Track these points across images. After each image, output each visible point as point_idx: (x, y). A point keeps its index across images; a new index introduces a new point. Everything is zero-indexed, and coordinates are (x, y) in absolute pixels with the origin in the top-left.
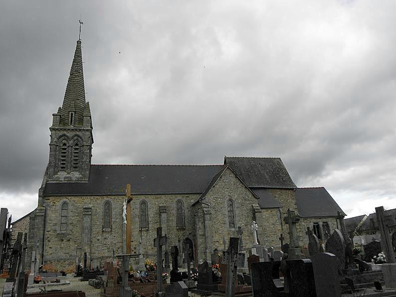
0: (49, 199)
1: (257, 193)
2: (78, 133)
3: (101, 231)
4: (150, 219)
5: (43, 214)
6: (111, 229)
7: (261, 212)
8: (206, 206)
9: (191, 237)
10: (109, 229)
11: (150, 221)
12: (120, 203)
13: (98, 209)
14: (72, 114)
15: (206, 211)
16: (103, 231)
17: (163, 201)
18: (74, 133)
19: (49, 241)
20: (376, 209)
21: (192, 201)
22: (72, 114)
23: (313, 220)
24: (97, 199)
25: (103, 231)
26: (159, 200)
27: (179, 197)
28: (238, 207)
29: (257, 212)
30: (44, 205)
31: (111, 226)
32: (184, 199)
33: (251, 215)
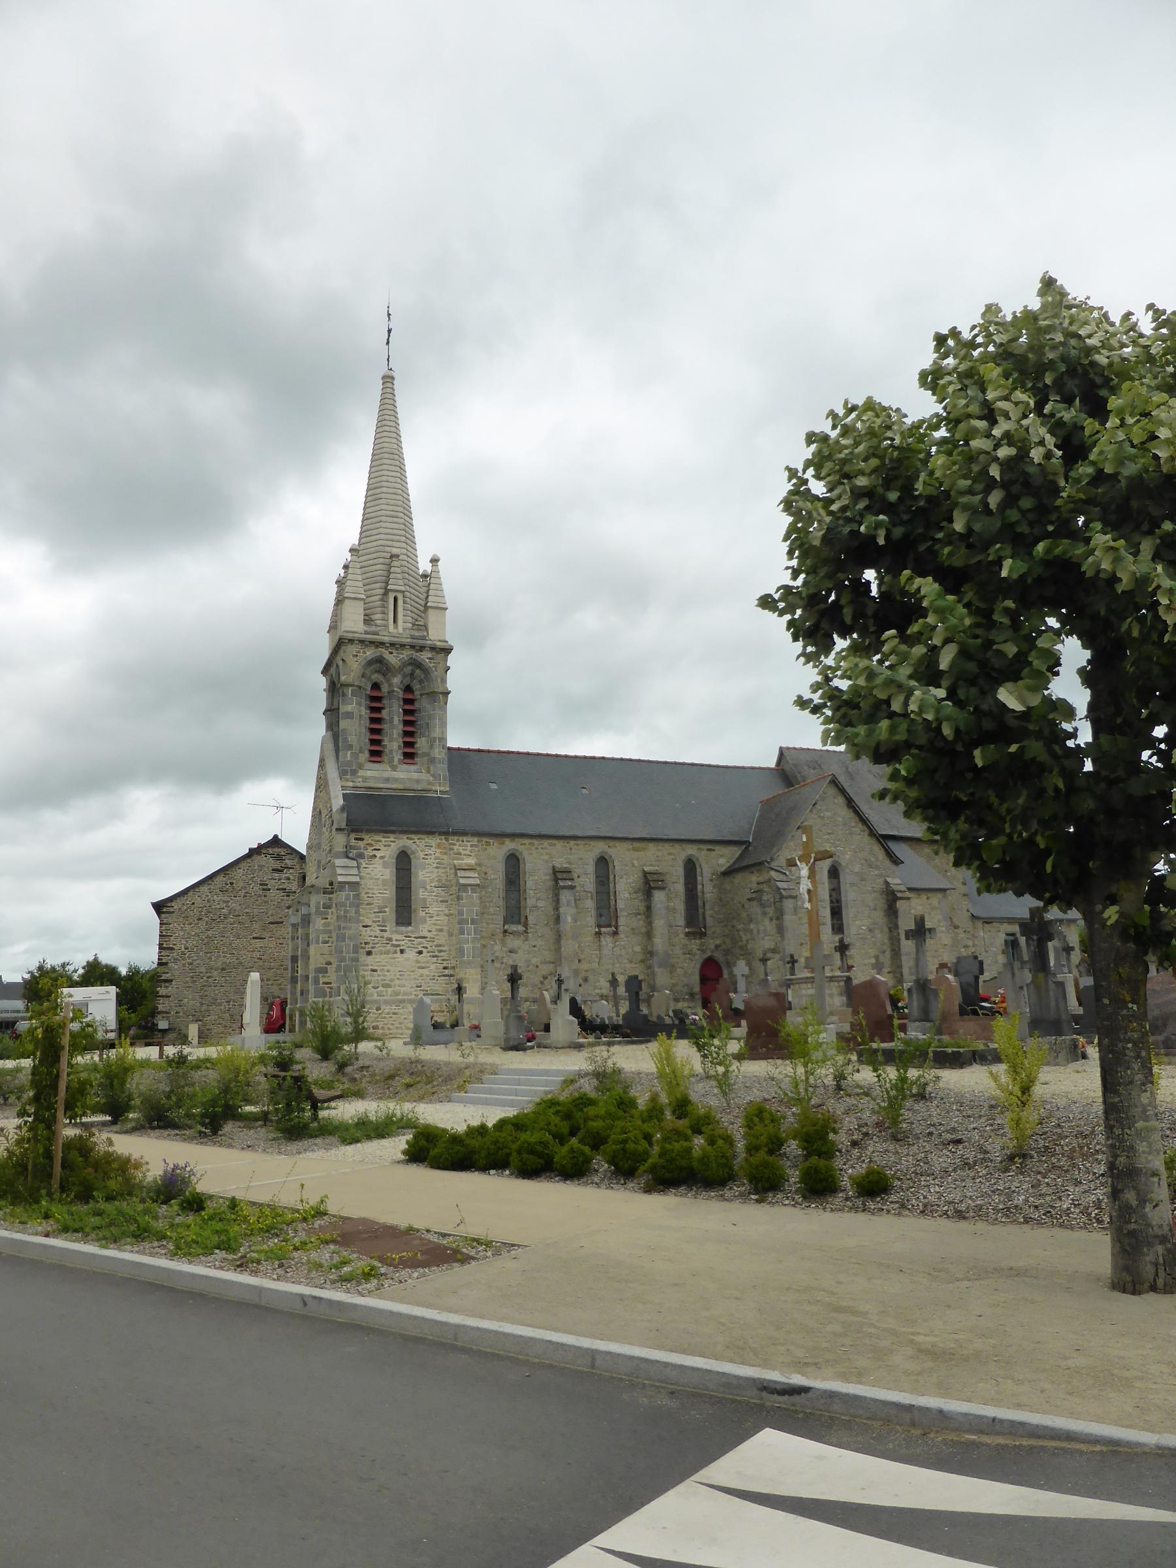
0: (362, 839)
1: (898, 849)
2: (416, 655)
3: (499, 931)
4: (621, 905)
5: (561, 883)
6: (526, 925)
7: (908, 899)
8: (782, 877)
9: (718, 956)
10: (520, 928)
11: (622, 910)
12: (546, 857)
13: (489, 872)
14: (396, 599)
15: (785, 889)
16: (505, 931)
17: (560, 855)
18: (406, 654)
19: (369, 953)
20: (782, 753)
21: (722, 861)
22: (396, 599)
23: (1005, 925)
24: (488, 844)
25: (505, 931)
26: (641, 854)
27: (691, 850)
28: (852, 884)
29: (786, 898)
30: (351, 855)
31: (523, 920)
32: (702, 856)
33: (882, 904)
